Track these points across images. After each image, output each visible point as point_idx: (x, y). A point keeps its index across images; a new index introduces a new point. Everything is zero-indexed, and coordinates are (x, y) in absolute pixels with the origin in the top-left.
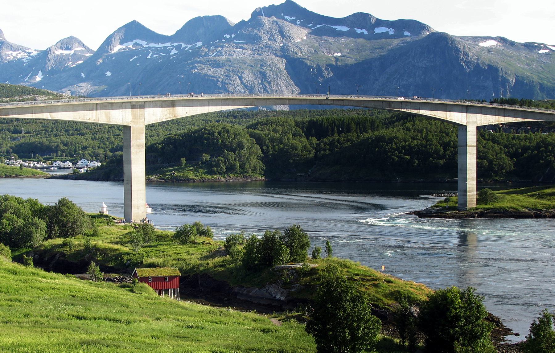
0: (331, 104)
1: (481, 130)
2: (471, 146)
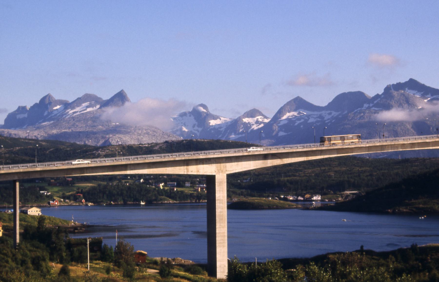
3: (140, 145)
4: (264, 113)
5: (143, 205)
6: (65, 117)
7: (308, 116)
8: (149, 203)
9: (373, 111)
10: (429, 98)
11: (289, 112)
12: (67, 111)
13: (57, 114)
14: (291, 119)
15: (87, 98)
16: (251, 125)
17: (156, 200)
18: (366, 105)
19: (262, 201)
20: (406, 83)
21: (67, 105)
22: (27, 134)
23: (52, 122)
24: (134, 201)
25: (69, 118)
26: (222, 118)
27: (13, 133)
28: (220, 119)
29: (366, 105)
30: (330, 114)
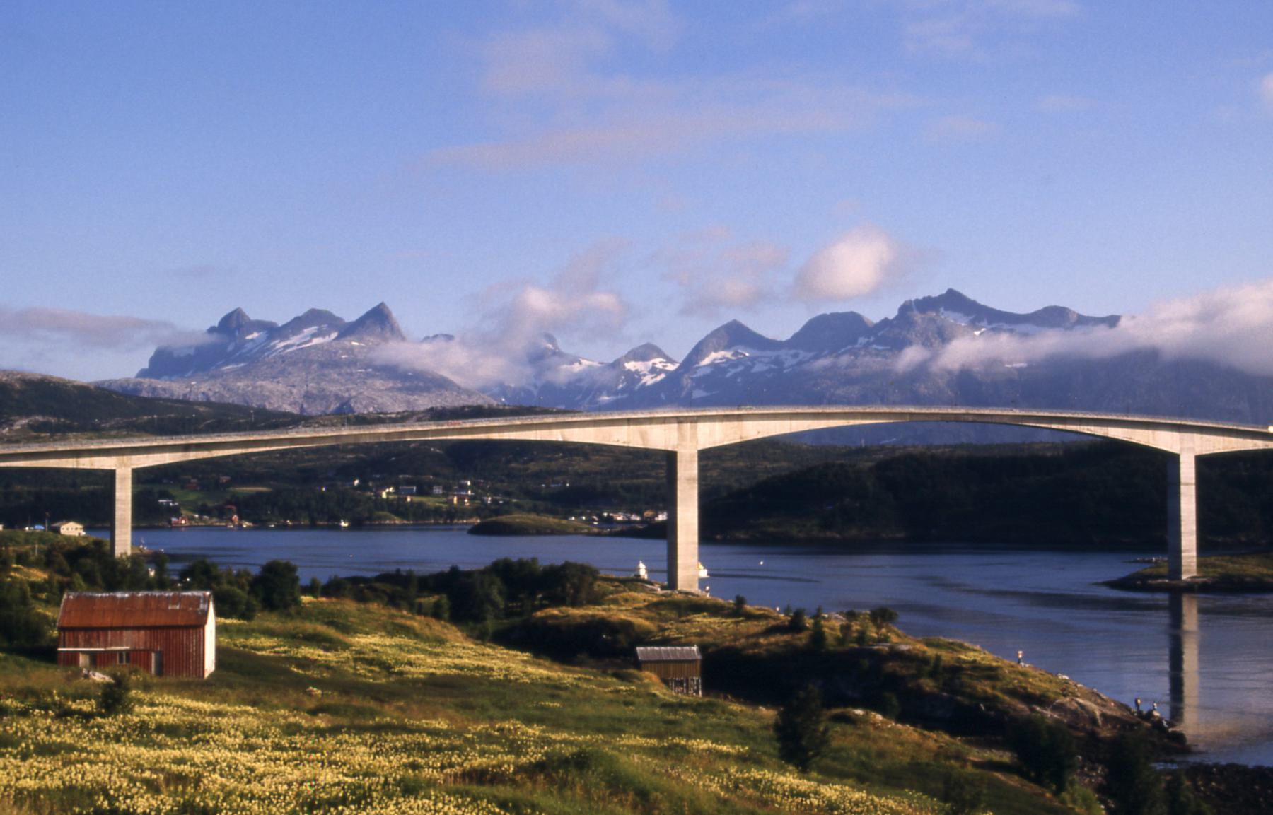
0: (973, 422)
1: (1204, 462)
2: (1187, 484)
3: (382, 416)
4: (667, 352)
5: (345, 527)
6: (268, 356)
7: (753, 360)
8: (357, 525)
9: (874, 352)
10: (983, 327)
11: (716, 351)
12: (272, 344)
13: (251, 350)
14: (718, 364)
15: (316, 318)
16: (640, 376)
17: (369, 518)
18: (862, 340)
19: (530, 522)
20: (941, 296)
21: (273, 331)
22: (188, 390)
23: (242, 365)
24: (328, 521)
25: (274, 357)
26: (585, 362)
27: (159, 386)
28: (580, 363)
29: (862, 340)
30: (796, 356)
